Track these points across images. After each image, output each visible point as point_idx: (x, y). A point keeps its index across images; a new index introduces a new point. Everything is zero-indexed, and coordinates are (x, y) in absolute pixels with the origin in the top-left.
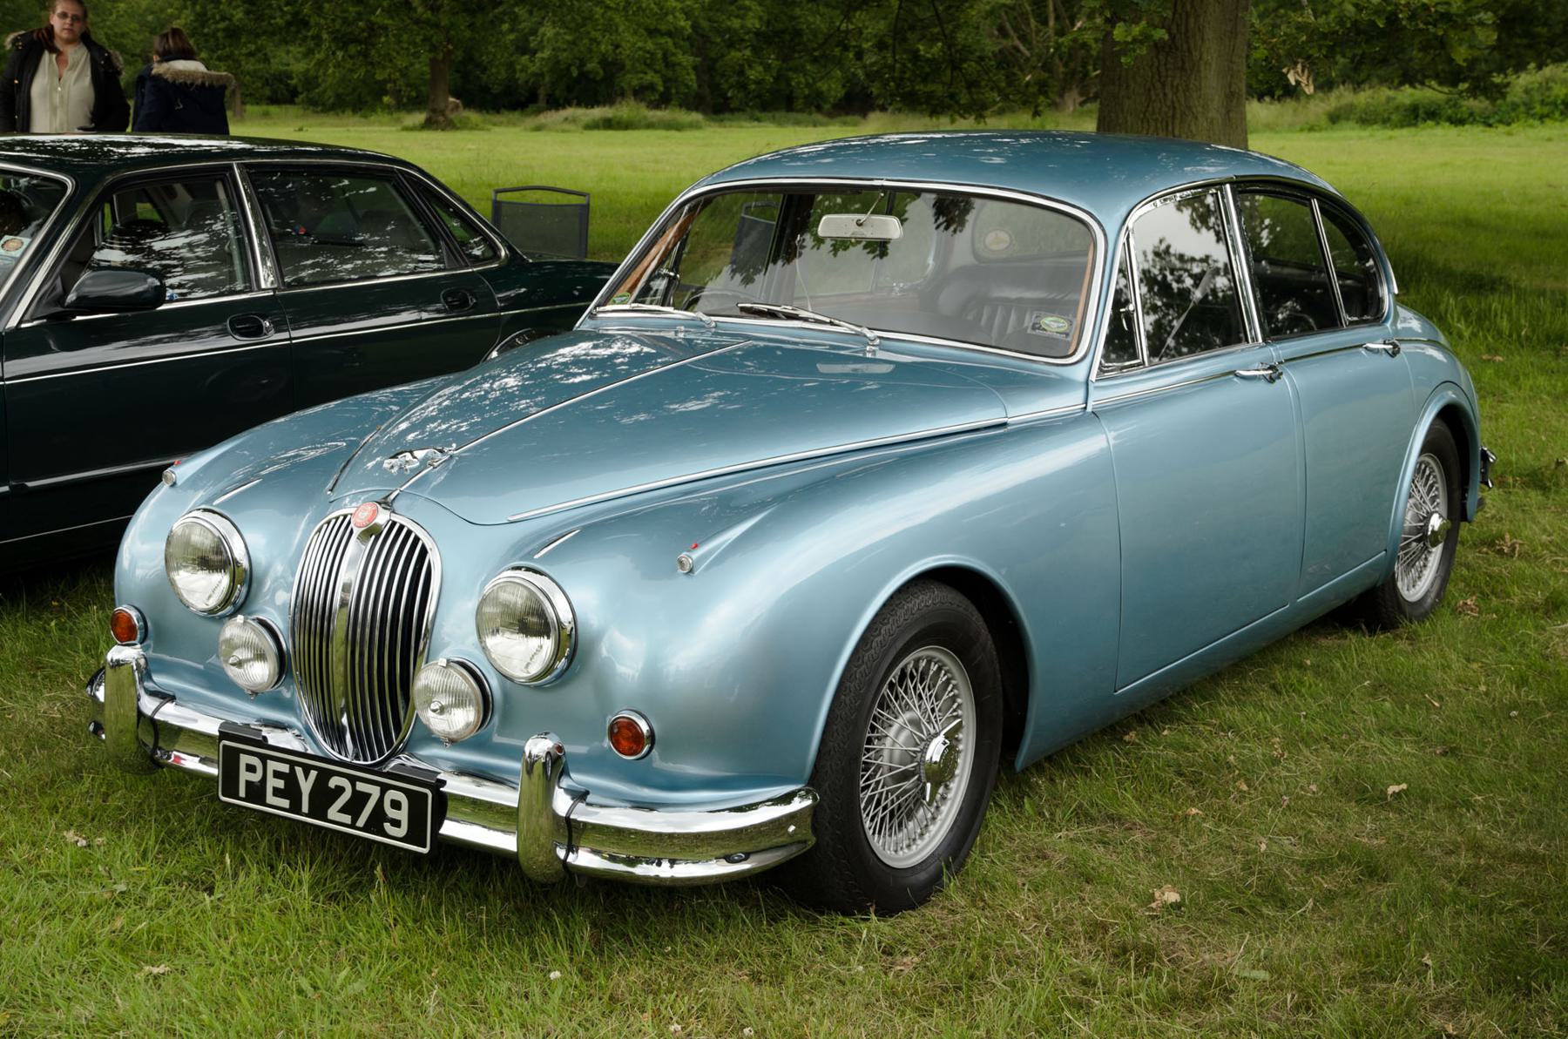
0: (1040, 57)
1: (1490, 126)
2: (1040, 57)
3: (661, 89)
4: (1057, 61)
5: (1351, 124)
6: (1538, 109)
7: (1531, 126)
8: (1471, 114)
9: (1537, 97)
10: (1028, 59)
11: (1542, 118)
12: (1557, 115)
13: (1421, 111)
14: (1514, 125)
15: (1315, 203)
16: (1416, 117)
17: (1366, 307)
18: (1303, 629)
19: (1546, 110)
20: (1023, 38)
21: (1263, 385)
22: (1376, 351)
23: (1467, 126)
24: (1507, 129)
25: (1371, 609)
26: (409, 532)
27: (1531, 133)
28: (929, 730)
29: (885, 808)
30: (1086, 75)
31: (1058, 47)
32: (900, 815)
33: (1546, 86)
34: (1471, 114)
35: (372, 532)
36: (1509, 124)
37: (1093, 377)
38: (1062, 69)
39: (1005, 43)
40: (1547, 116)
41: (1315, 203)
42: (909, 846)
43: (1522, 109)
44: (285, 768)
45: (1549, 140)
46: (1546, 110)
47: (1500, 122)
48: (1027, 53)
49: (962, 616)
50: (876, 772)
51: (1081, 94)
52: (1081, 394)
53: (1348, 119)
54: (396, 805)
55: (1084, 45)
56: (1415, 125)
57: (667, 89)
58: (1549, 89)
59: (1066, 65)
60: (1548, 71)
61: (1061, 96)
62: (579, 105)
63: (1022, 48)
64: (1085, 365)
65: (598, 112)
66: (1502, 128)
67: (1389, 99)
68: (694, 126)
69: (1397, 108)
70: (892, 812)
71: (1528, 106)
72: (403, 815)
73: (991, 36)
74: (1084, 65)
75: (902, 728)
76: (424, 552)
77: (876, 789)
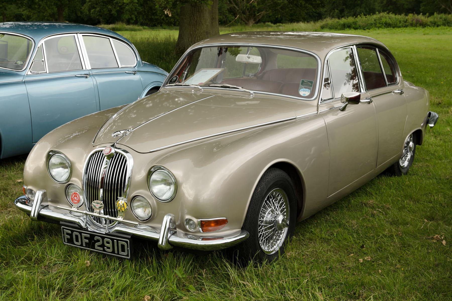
0: (241, 9)
1: (365, 30)
2: (241, 9)
3: (135, 19)
4: (247, 11)
5: (327, 29)
6: (378, 25)
7: (375, 30)
8: (360, 26)
9: (378, 21)
10: (238, 10)
11: (379, 27)
12: (383, 27)
13: (346, 26)
14: (371, 30)
15: (377, 49)
16: (345, 27)
17: (392, 80)
18: (378, 176)
19: (380, 25)
20: (237, 5)
21: (366, 105)
22: (396, 93)
23: (358, 30)
24: (369, 30)
25: (393, 170)
26: (124, 157)
27: (375, 32)
28: (275, 213)
29: (265, 238)
30: (255, 15)
31: (246, 7)
32: (268, 239)
33: (380, 19)
34: (360, 26)
35: (110, 157)
36: (369, 29)
37: (319, 103)
38: (248, 13)
39: (232, 6)
40: (380, 27)
41: (377, 49)
42: (271, 248)
43: (374, 25)
44: (70, 232)
45: (379, 34)
46: (380, 25)
47: (368, 29)
48: (238, 9)
49: (284, 179)
50: (262, 227)
51: (254, 21)
52: (316, 108)
53: (326, 28)
54: (108, 243)
55: (254, 6)
56: (344, 30)
57: (136, 19)
58: (381, 19)
59: (249, 12)
60: (382, 14)
61: (248, 21)
62: (105, 24)
63: (236, 7)
64: (317, 100)
65: (111, 26)
66: (368, 30)
67: (338, 22)
68: (140, 30)
69: (339, 25)
70: (267, 239)
71: (375, 24)
72: (110, 245)
73: (226, 3)
74: (254, 12)
75: (269, 213)
76: (126, 161)
77: (262, 232)
